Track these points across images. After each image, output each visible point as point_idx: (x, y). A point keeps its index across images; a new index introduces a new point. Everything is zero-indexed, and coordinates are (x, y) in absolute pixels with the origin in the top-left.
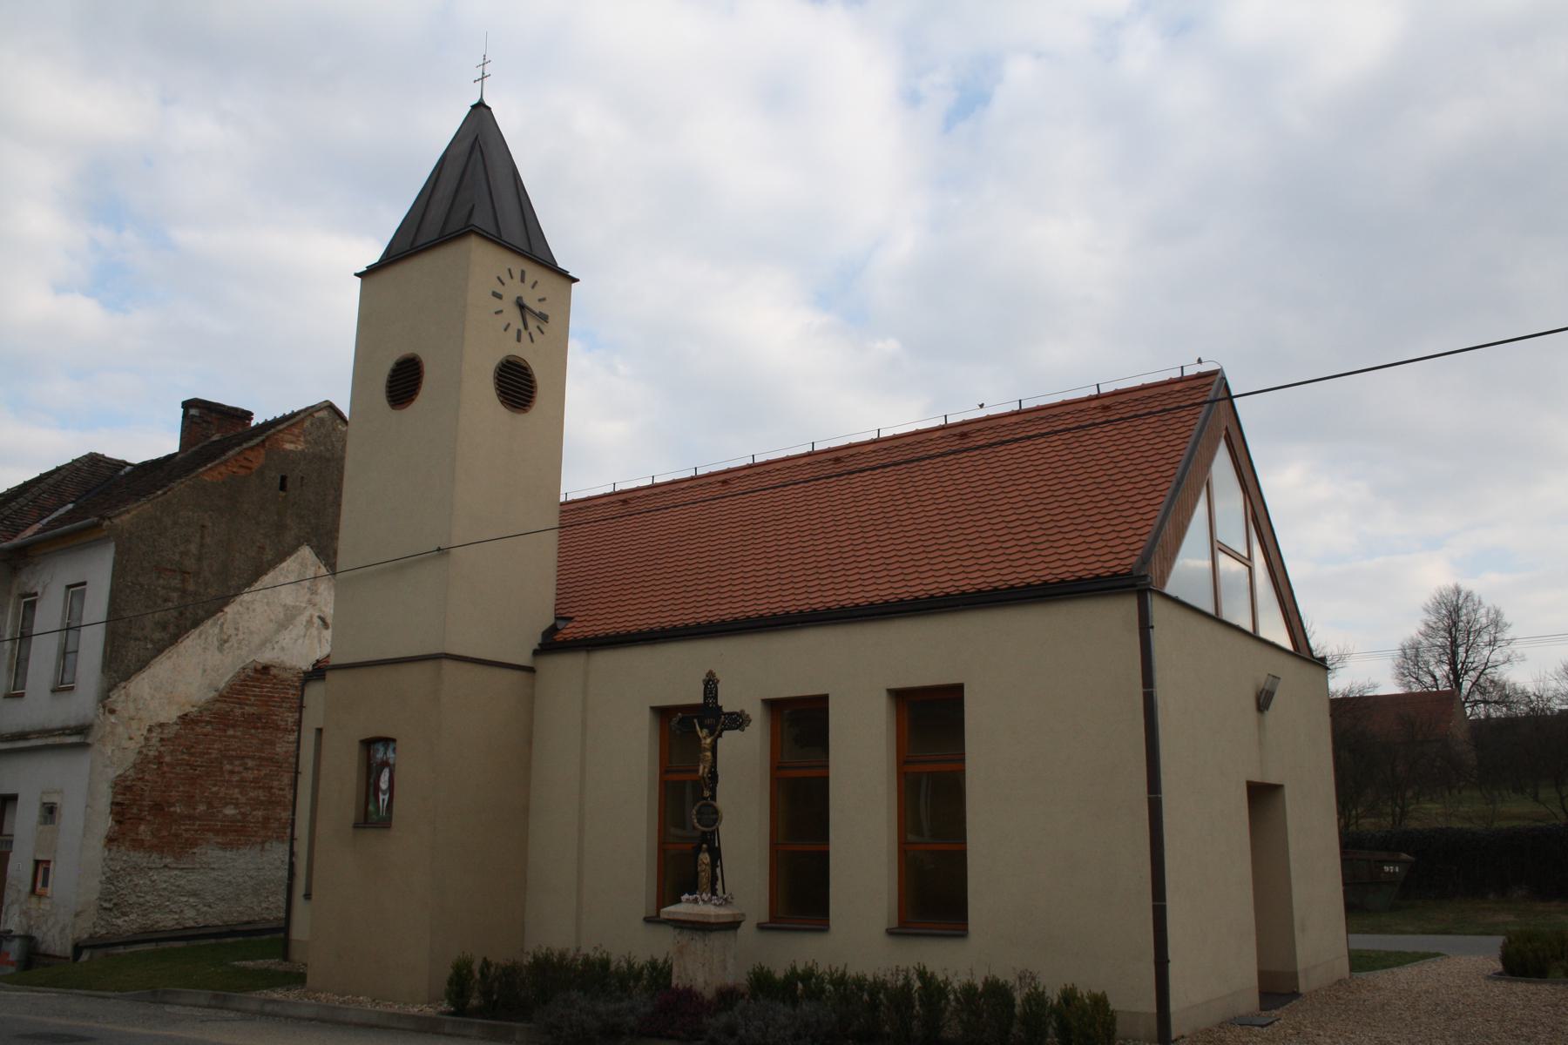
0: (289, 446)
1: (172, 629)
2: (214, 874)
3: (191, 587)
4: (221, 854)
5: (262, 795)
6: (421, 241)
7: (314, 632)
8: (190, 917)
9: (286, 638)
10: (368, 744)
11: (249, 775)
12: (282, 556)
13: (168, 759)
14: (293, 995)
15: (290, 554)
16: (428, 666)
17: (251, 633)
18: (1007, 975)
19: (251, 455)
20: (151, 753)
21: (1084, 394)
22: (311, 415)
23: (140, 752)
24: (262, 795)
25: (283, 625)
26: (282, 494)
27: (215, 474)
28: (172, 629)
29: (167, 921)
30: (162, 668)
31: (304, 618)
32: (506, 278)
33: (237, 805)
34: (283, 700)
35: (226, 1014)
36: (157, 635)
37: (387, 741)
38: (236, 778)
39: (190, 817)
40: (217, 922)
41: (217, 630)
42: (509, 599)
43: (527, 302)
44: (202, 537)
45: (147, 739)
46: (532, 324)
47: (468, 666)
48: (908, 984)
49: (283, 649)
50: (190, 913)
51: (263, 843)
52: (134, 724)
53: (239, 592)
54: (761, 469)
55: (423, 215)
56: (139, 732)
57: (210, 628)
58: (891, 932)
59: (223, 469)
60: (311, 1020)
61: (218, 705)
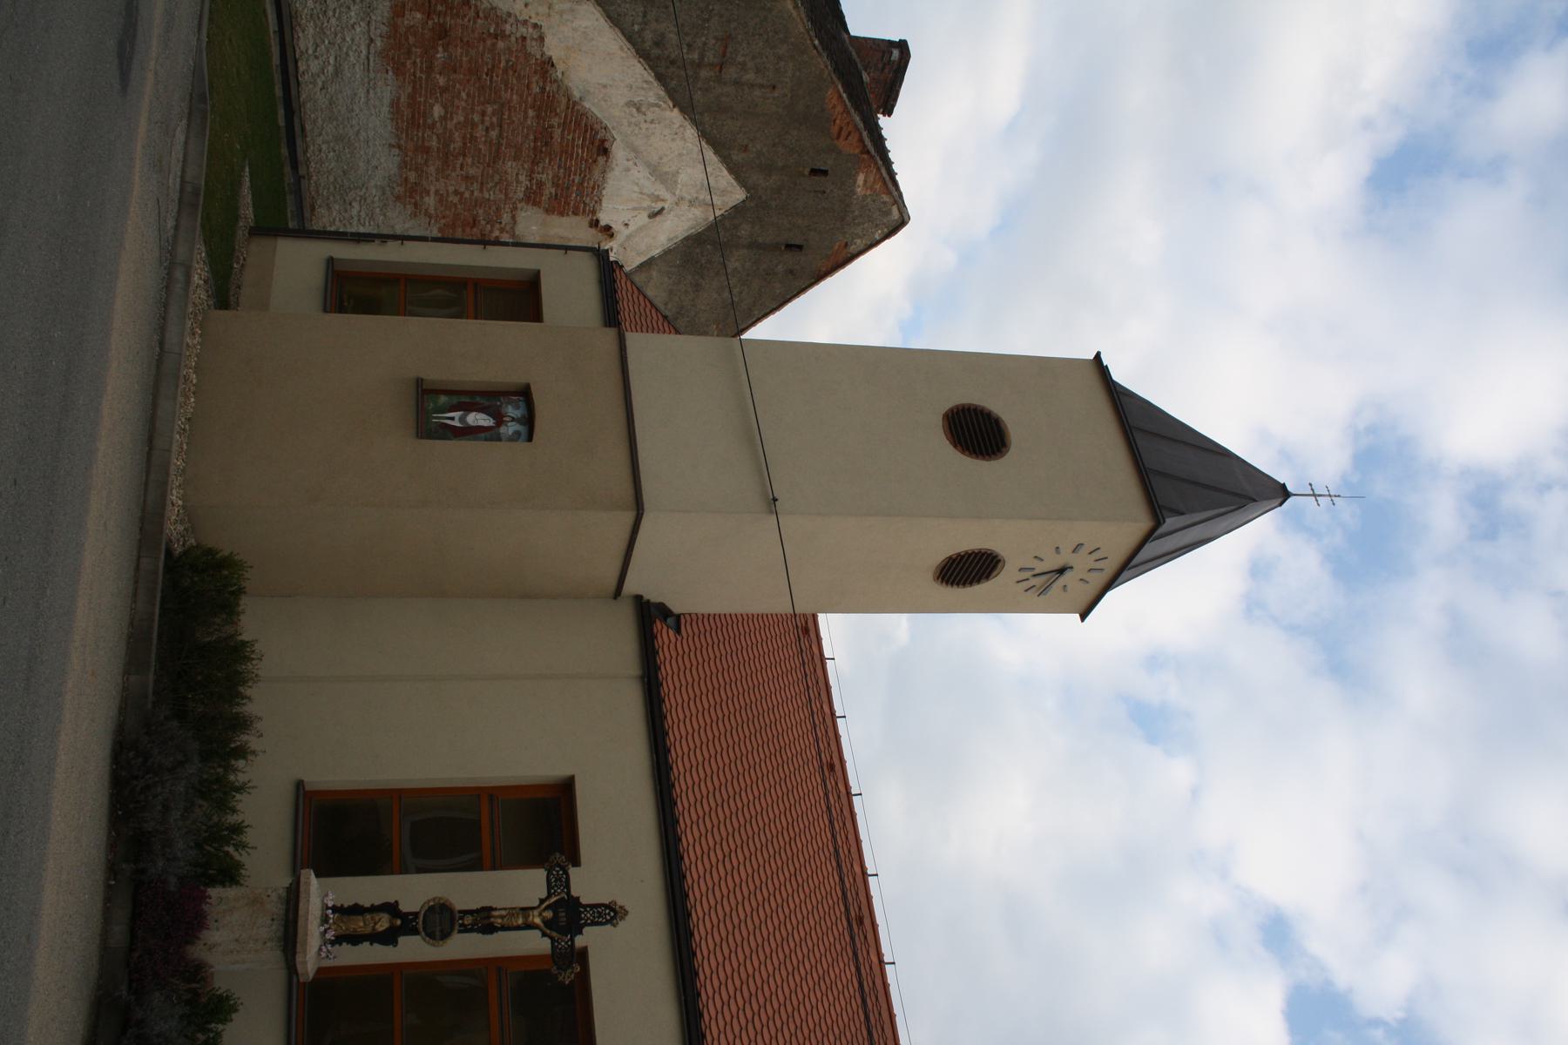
0: (861, 178)
1: (656, 52)
2: (361, 93)
3: (704, 73)
4: (387, 101)
5: (457, 145)
6: (1138, 436)
7: (646, 203)
8: (309, 67)
9: (640, 174)
10: (525, 394)
11: (480, 132)
12: (734, 170)
13: (501, 45)
14: (200, 295)
15: (737, 179)
16: (624, 489)
17: (648, 137)
18: (249, 837)
19: (854, 139)
20: (508, 27)
21: (885, 949)
22: (896, 202)
23: (509, 15)
24: (457, 145)
25: (656, 171)
26: (807, 172)
27: (834, 101)
28: (656, 52)
29: (305, 40)
30: (610, 41)
31: (662, 192)
32: (1096, 555)
33: (444, 118)
34: (568, 170)
35: (174, 207)
36: (648, 35)
37: (529, 421)
38: (476, 118)
39: (430, 68)
40: (303, 96)
41: (652, 100)
42: (702, 561)
43: (1068, 574)
44: (762, 86)
45: (525, 22)
46: (1038, 581)
47: (626, 536)
48: (234, 811)
49: (628, 170)
50: (315, 66)
51: (399, 147)
52: (543, 9)
53: (696, 123)
54: (861, 886)
55: (1164, 437)
56: (535, 13)
57: (655, 93)
58: (299, 785)
59: (839, 109)
60: (161, 343)
61: (564, 101)
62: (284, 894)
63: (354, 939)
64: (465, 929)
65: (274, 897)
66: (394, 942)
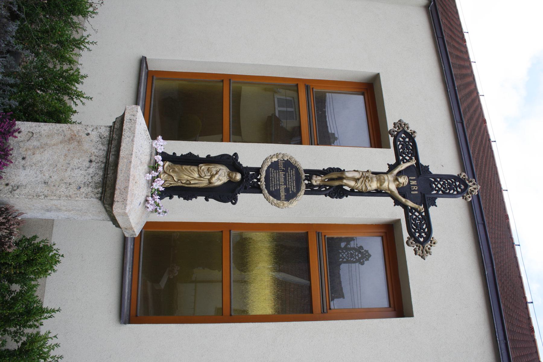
62: (106, 133)
63: (188, 192)
64: (312, 190)
65: (94, 135)
66: (234, 200)
